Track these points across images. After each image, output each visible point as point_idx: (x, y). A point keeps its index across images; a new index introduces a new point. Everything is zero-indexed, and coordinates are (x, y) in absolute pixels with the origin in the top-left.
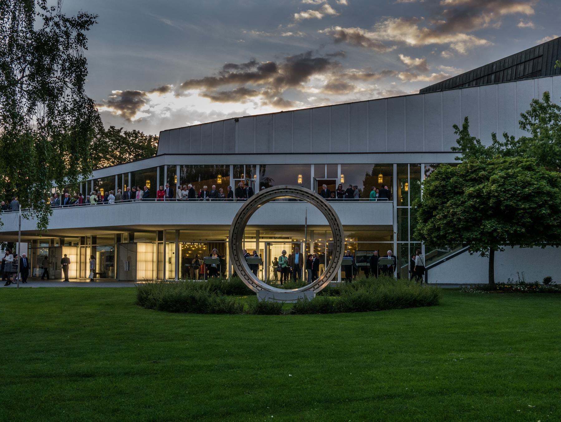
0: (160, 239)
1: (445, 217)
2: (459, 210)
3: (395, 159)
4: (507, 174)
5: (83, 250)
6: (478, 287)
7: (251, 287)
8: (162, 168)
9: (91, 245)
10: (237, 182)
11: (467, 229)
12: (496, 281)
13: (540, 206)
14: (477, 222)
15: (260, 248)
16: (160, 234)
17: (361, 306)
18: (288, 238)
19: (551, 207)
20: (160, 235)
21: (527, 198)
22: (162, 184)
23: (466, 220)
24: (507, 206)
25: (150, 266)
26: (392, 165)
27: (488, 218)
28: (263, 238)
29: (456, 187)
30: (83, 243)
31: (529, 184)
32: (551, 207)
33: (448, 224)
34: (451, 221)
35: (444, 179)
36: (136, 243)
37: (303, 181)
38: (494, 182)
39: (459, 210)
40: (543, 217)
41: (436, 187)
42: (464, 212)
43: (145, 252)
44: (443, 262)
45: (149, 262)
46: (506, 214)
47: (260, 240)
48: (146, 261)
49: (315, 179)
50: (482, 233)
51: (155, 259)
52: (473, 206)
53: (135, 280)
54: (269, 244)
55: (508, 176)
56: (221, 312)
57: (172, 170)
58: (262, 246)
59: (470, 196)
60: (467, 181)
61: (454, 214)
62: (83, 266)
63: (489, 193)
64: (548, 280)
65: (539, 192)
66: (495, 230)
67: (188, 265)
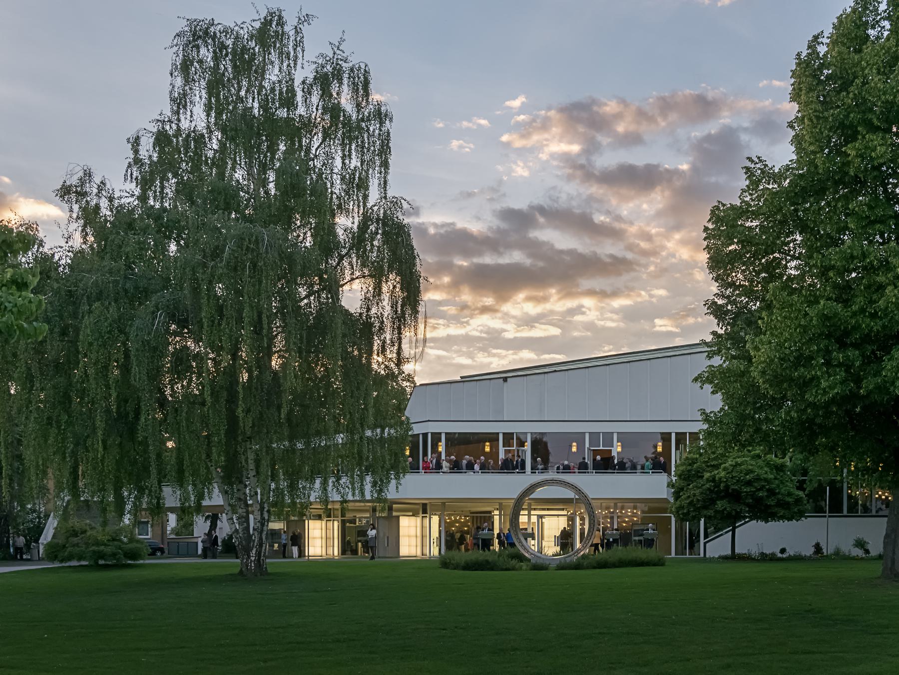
0: (425, 512)
1: (689, 497)
2: (697, 492)
3: (673, 428)
4: (736, 462)
5: (330, 524)
6: (725, 558)
7: (527, 555)
8: (425, 435)
9: (340, 519)
10: (507, 452)
11: (705, 507)
12: (738, 551)
13: (759, 490)
14: (713, 502)
15: (532, 521)
16: (424, 506)
17: (603, 565)
18: (563, 509)
19: (768, 490)
20: (423, 509)
21: (749, 483)
22: (425, 454)
23: (704, 500)
24: (733, 489)
25: (413, 541)
26: (670, 433)
27: (722, 498)
28: (535, 509)
29: (699, 472)
30: (329, 516)
31: (752, 471)
32: (768, 490)
33: (691, 503)
34: (692, 501)
35: (690, 465)
36: (398, 517)
37: (577, 449)
38: (725, 469)
39: (697, 492)
40: (761, 498)
41: (683, 471)
42: (702, 493)
43: (409, 526)
44: (722, 535)
45: (415, 538)
46: (735, 497)
47: (533, 512)
48: (409, 536)
49: (589, 449)
50: (716, 512)
51: (419, 534)
52: (709, 489)
53: (398, 556)
54: (540, 517)
55: (737, 464)
56: (507, 569)
57: (436, 437)
58: (534, 519)
59: (708, 480)
60: (708, 466)
61: (694, 495)
62: (330, 542)
63: (720, 479)
64: (783, 551)
65: (758, 479)
66: (725, 509)
67: (451, 540)
